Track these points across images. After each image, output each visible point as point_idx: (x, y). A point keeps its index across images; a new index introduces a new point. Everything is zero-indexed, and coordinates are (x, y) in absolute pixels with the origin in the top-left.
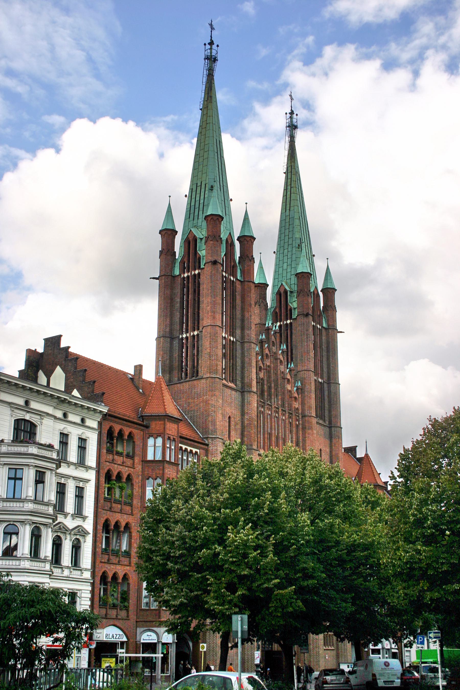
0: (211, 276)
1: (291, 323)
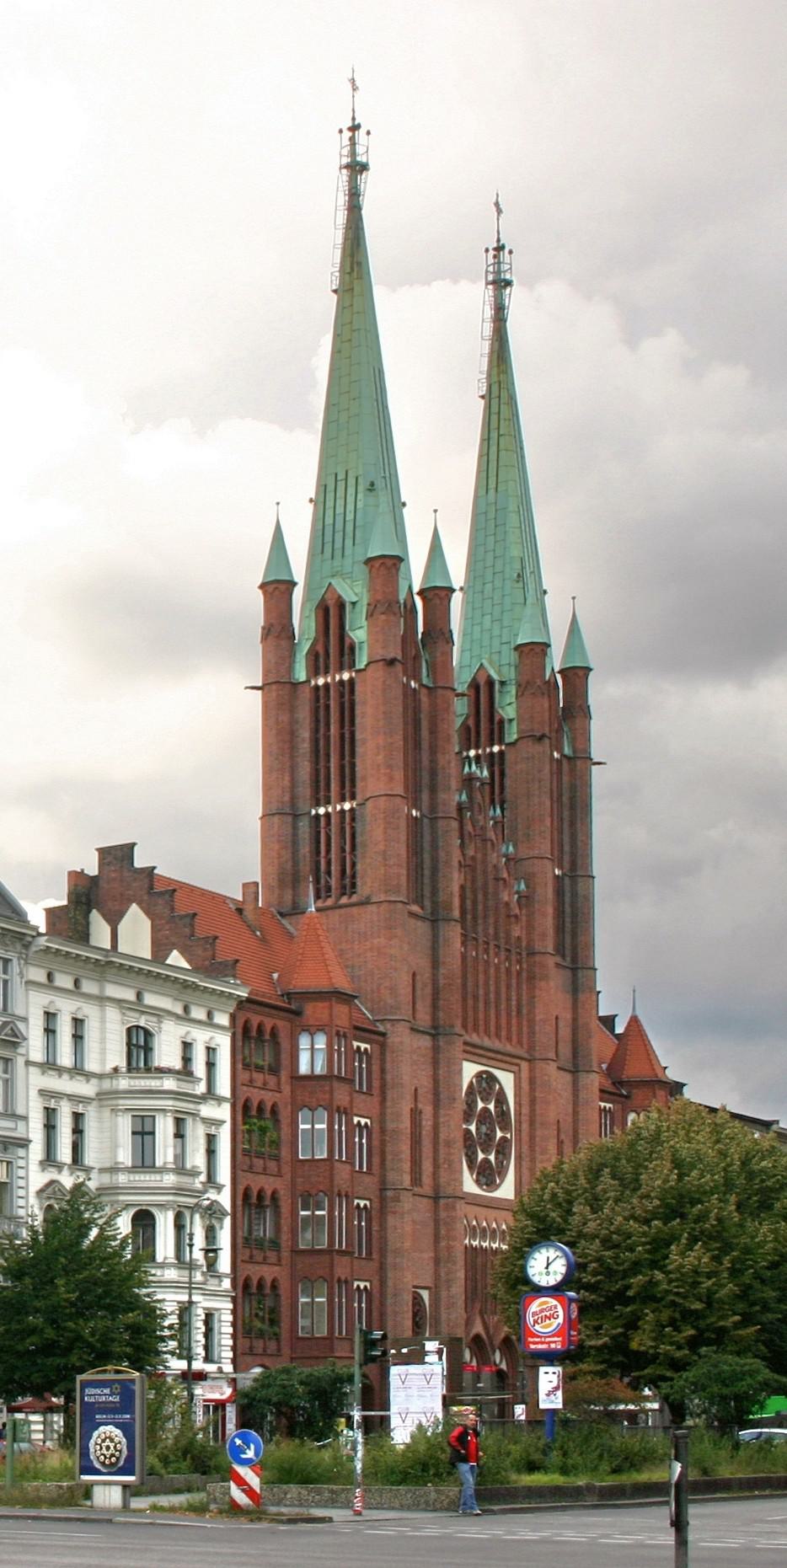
0: (384, 690)
1: (501, 753)
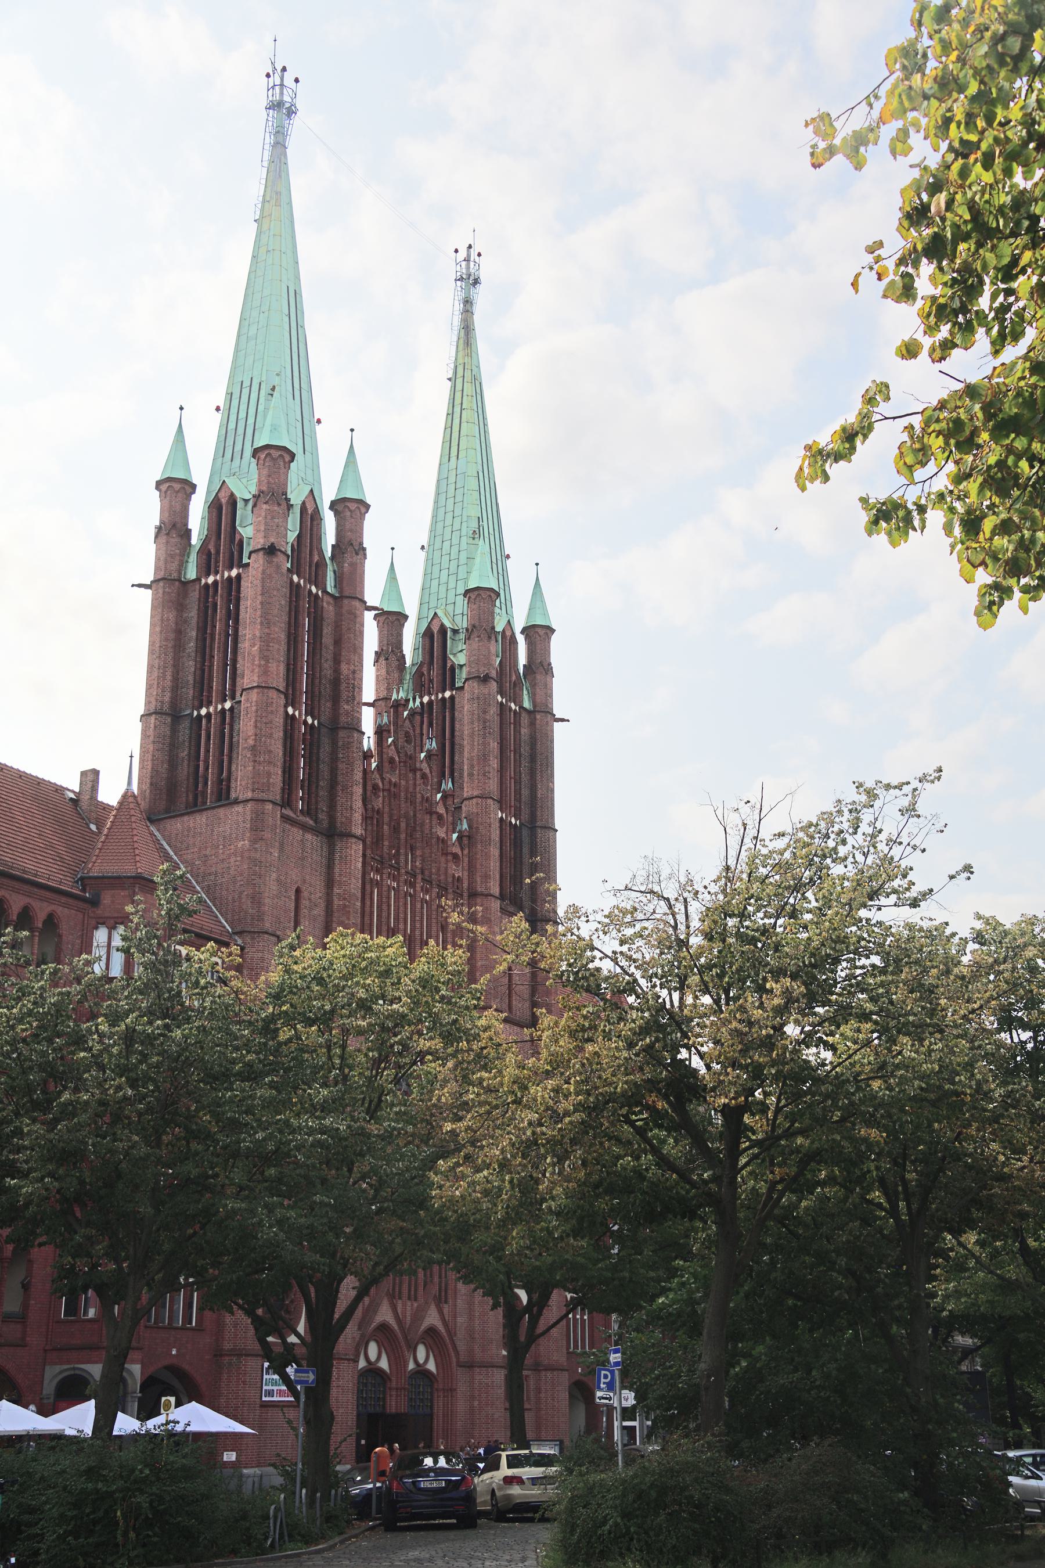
1: (452, 697)
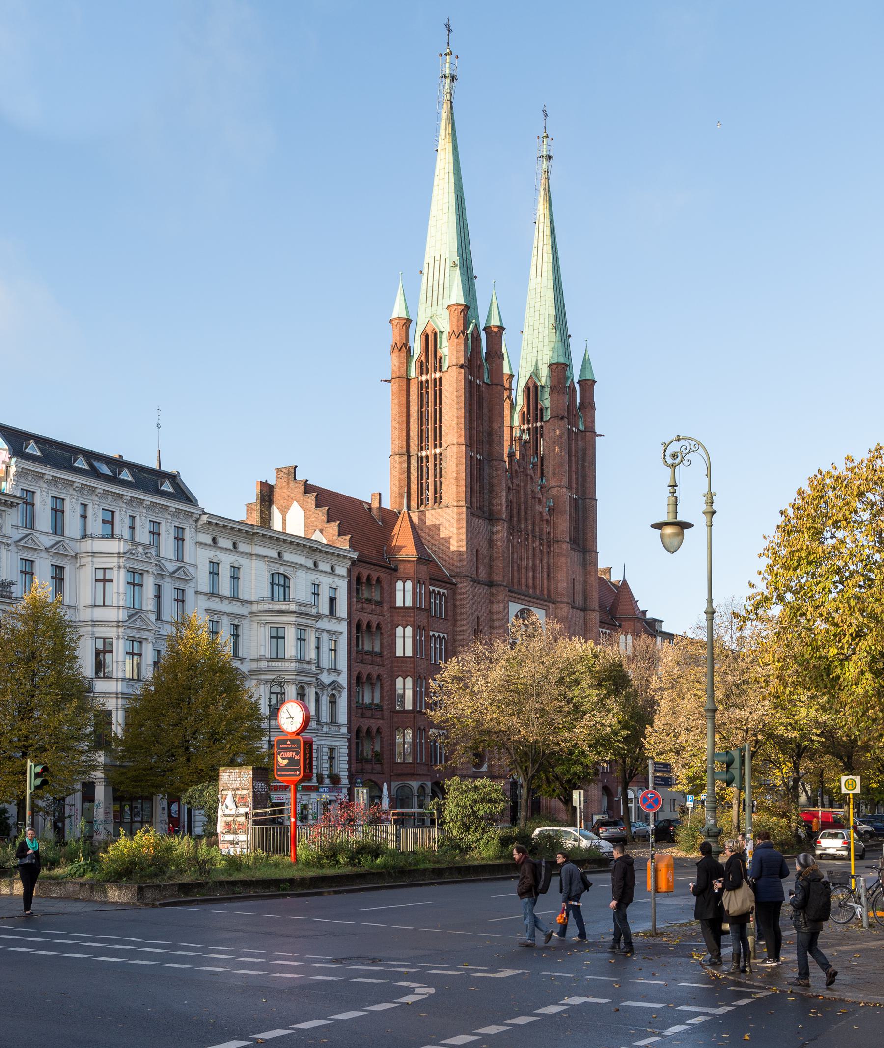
1: (542, 427)
